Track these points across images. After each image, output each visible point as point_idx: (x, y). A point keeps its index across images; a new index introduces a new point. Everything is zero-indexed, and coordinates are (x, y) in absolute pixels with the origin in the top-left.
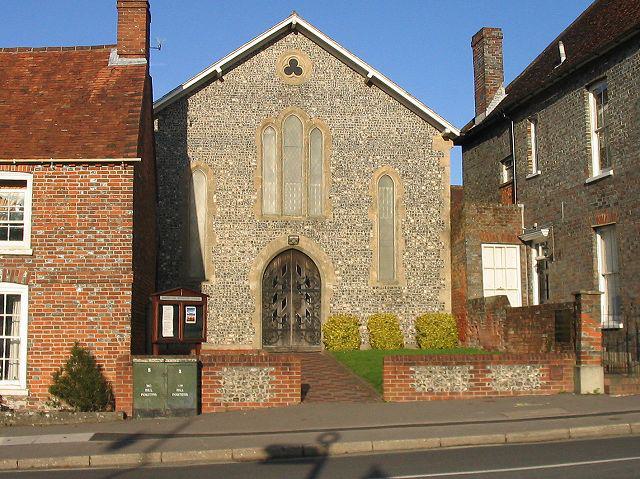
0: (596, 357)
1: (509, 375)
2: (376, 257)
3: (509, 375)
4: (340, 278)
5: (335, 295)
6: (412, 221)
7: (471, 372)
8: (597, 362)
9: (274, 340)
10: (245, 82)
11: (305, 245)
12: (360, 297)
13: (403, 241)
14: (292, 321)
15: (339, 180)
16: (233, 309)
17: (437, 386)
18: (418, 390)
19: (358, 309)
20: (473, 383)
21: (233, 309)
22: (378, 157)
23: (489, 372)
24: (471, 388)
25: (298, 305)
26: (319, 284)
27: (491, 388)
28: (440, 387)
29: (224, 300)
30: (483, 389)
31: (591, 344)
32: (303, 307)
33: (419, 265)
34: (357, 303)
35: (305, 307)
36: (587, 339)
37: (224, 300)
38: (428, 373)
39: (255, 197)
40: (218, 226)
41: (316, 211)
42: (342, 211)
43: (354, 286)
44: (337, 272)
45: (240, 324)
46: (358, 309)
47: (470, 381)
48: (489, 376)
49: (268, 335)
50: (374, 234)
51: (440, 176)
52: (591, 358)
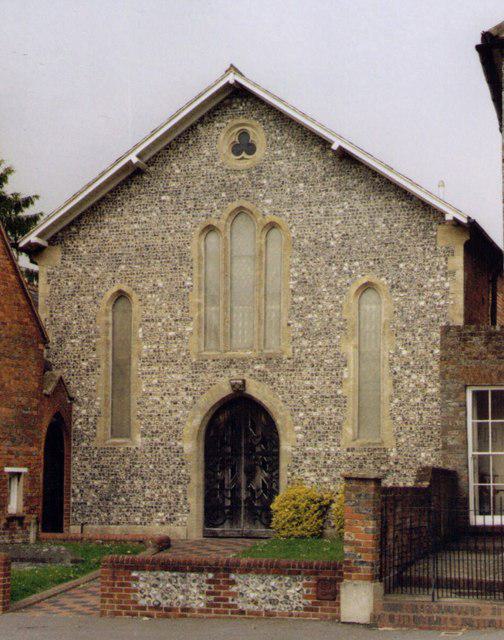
0: (365, 570)
1: (261, 587)
2: (351, 410)
3: (261, 587)
4: (301, 436)
5: (295, 459)
6: (404, 352)
7: (209, 581)
8: (365, 578)
9: (220, 521)
10: (178, 171)
11: (255, 390)
12: (329, 462)
13: (390, 382)
14: (244, 495)
15: (301, 298)
16: (162, 478)
17: (166, 598)
18: (142, 602)
19: (326, 479)
20: (212, 598)
21: (162, 478)
22: (357, 264)
23: (233, 583)
24: (209, 604)
25: (251, 474)
26: (277, 446)
27: (235, 606)
28: (169, 601)
29: (151, 467)
30: (225, 606)
31: (357, 551)
32: (257, 477)
33: (413, 416)
34: (324, 471)
35: (261, 477)
36: (353, 543)
37: (151, 467)
38: (155, 582)
39: (189, 329)
40: (145, 369)
41: (273, 347)
42: (305, 343)
43: (321, 447)
44: (298, 428)
45: (172, 500)
46: (326, 479)
47: (208, 594)
48: (234, 589)
49: (214, 513)
50: (349, 373)
51: (447, 285)
52: (358, 570)
